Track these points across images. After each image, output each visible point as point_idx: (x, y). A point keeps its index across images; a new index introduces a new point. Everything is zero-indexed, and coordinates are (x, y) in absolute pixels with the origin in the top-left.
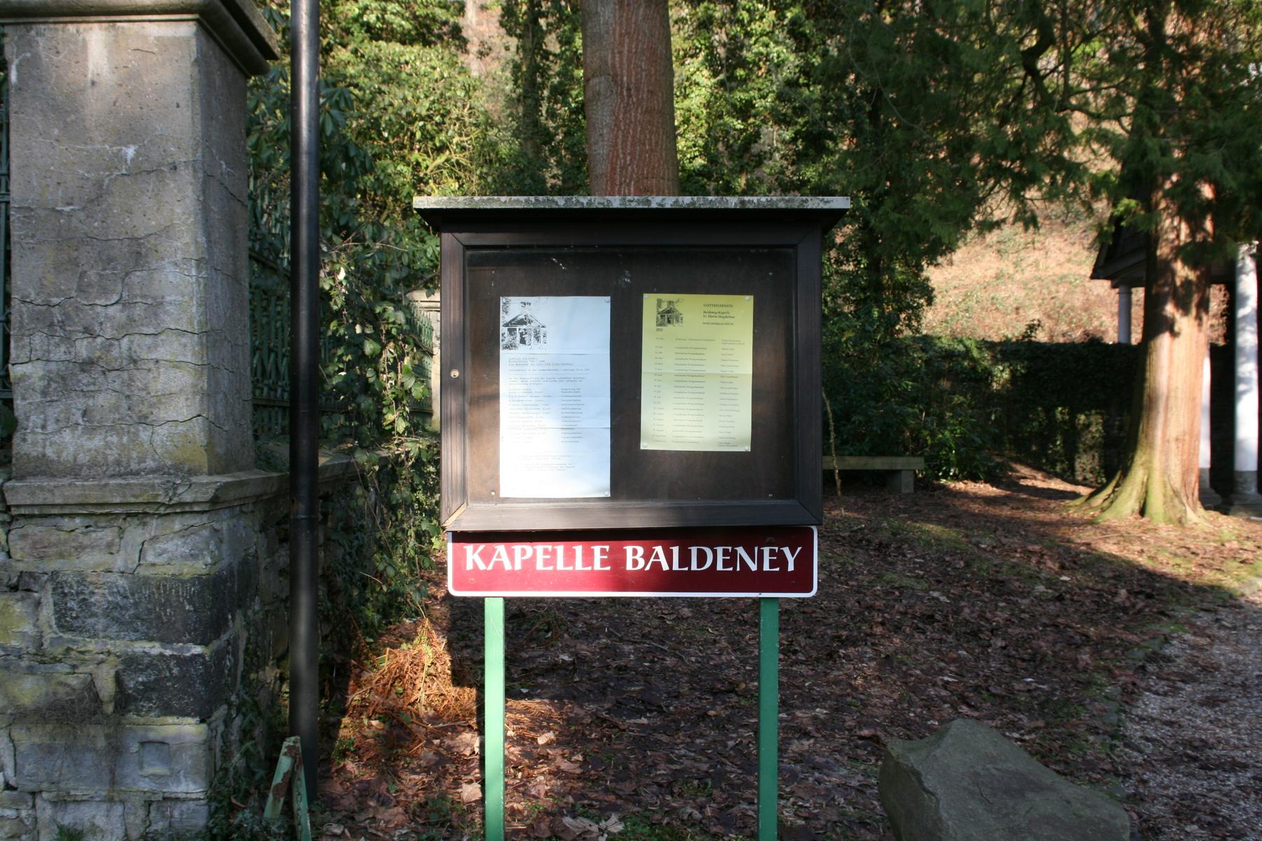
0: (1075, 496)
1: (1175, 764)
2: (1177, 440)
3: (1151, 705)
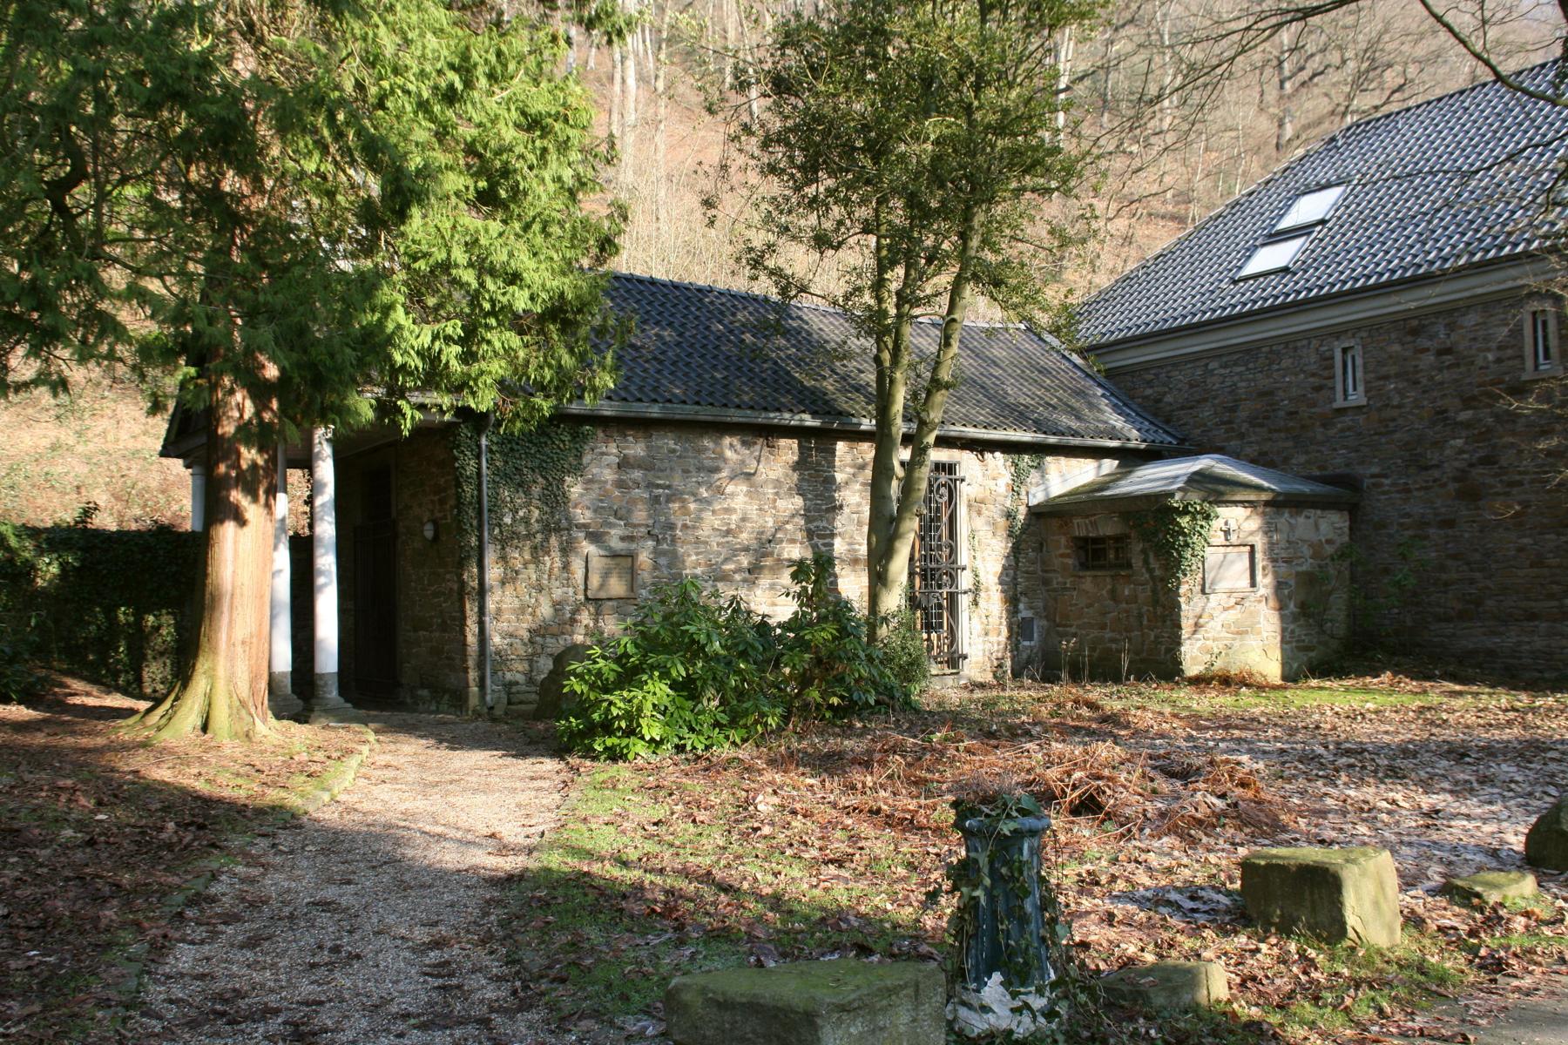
0: (131, 712)
1: (200, 1025)
2: (243, 643)
3: (184, 958)
